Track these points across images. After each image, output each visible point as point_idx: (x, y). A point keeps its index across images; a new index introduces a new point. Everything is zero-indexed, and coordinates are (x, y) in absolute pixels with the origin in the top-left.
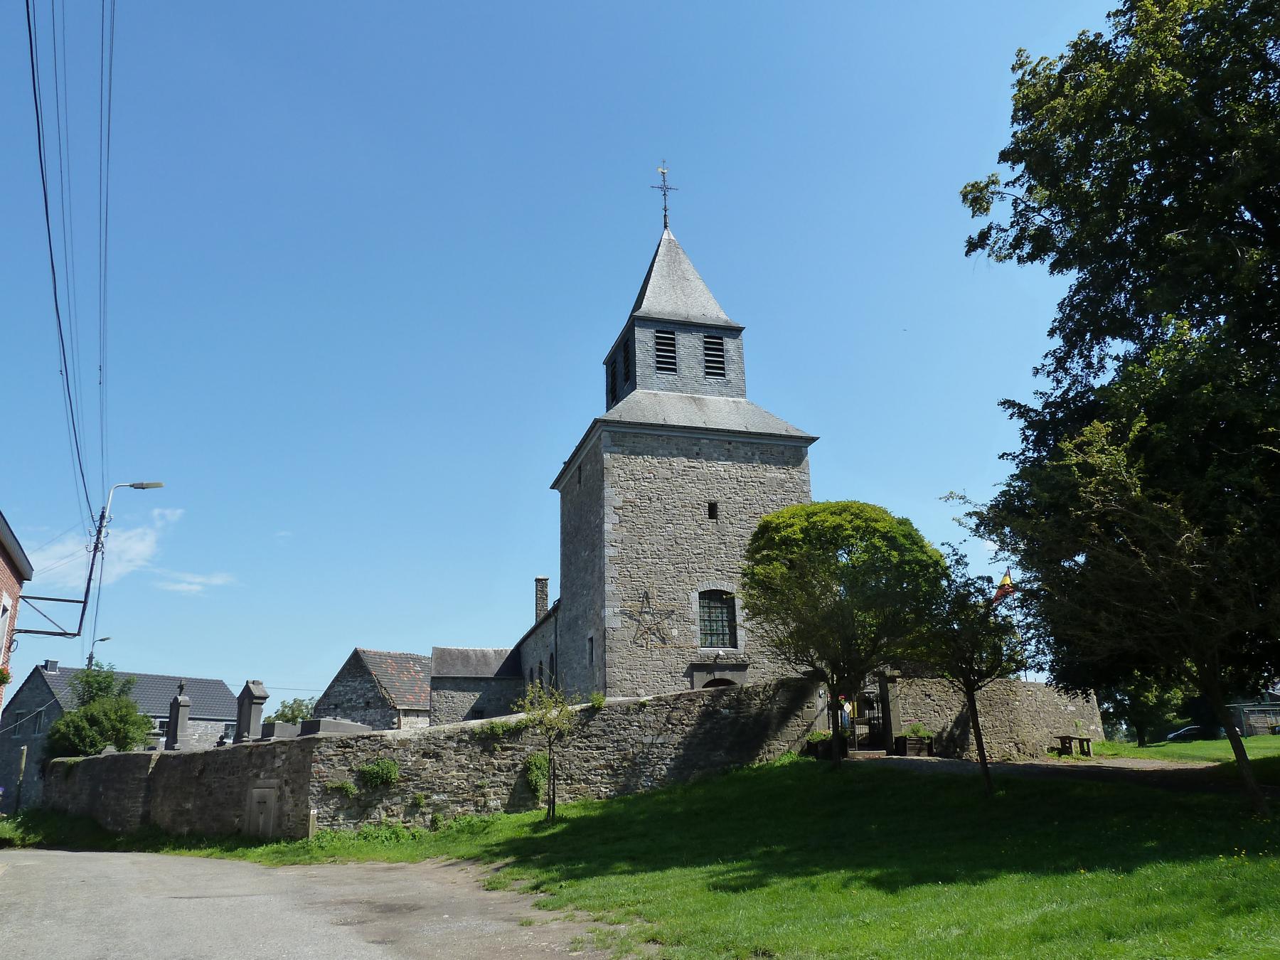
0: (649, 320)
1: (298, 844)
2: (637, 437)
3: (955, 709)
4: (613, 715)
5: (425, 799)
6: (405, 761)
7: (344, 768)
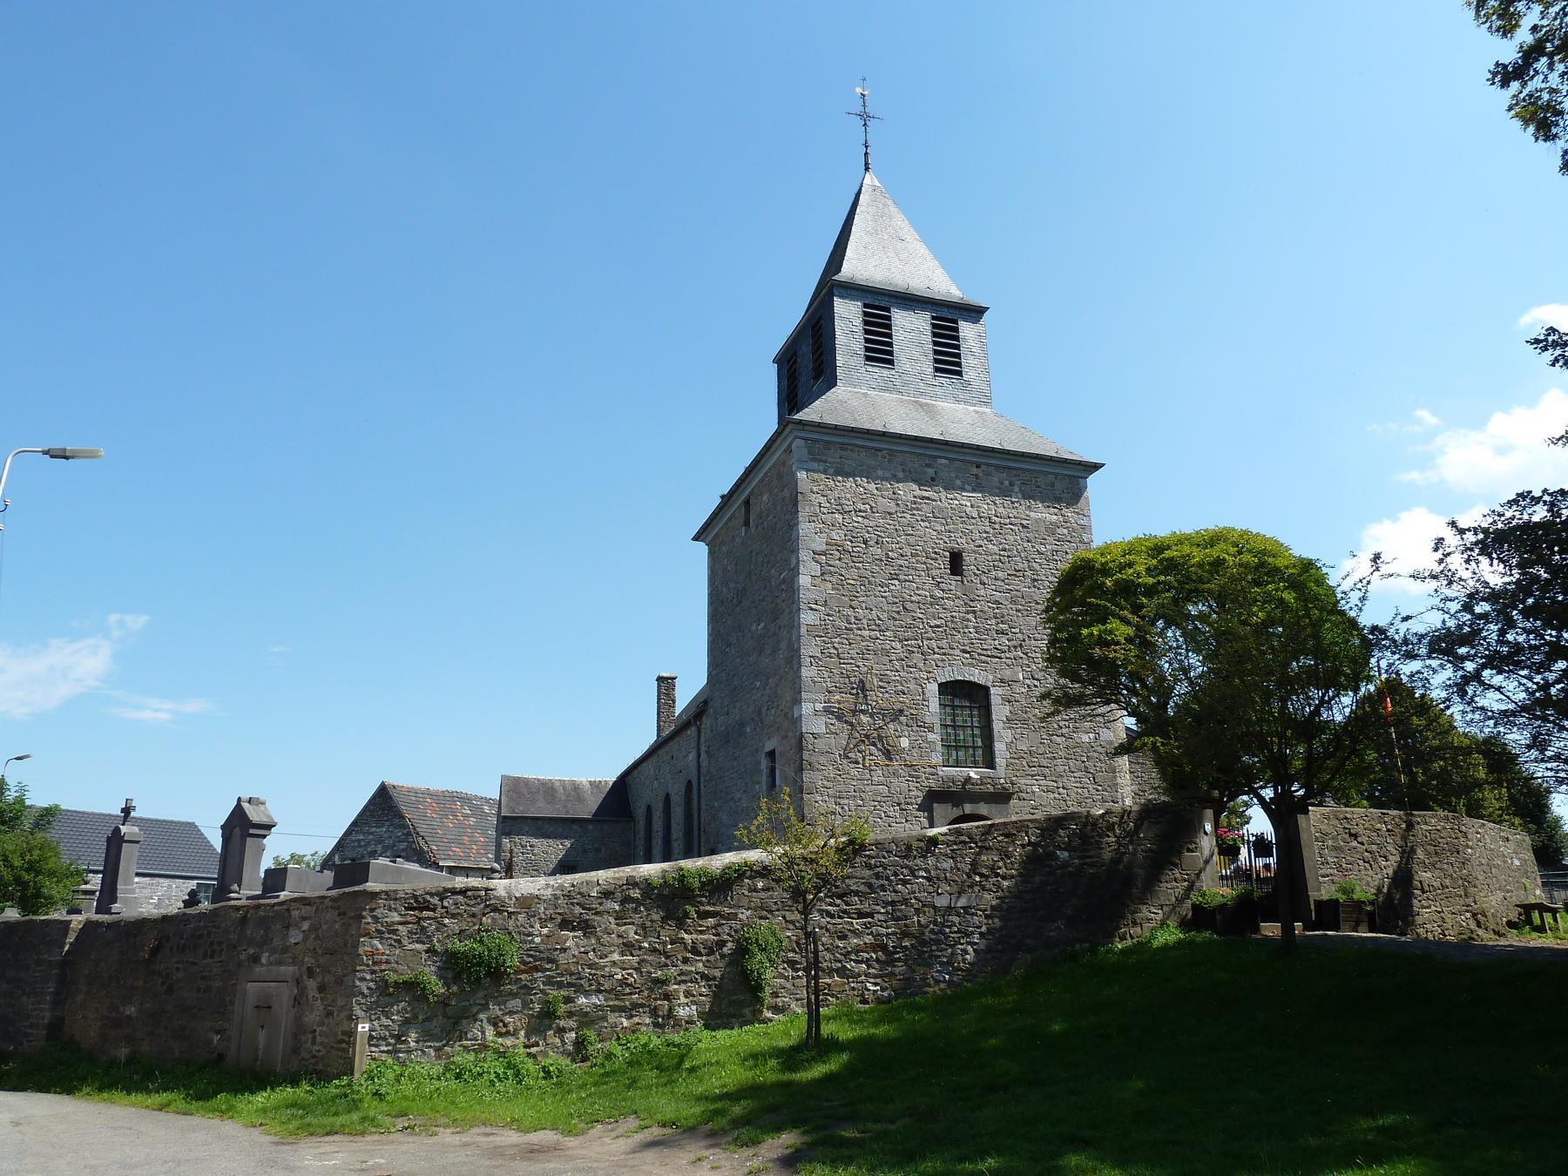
0: (854, 289)
1: (332, 1089)
2: (846, 450)
3: (1391, 857)
4: (885, 858)
5: (565, 1003)
6: (530, 934)
7: (418, 946)
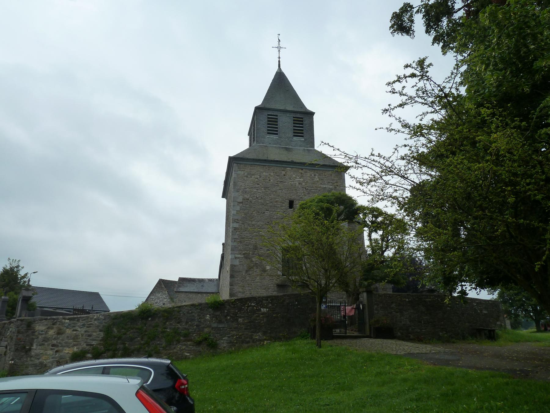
2: (252, 166)
